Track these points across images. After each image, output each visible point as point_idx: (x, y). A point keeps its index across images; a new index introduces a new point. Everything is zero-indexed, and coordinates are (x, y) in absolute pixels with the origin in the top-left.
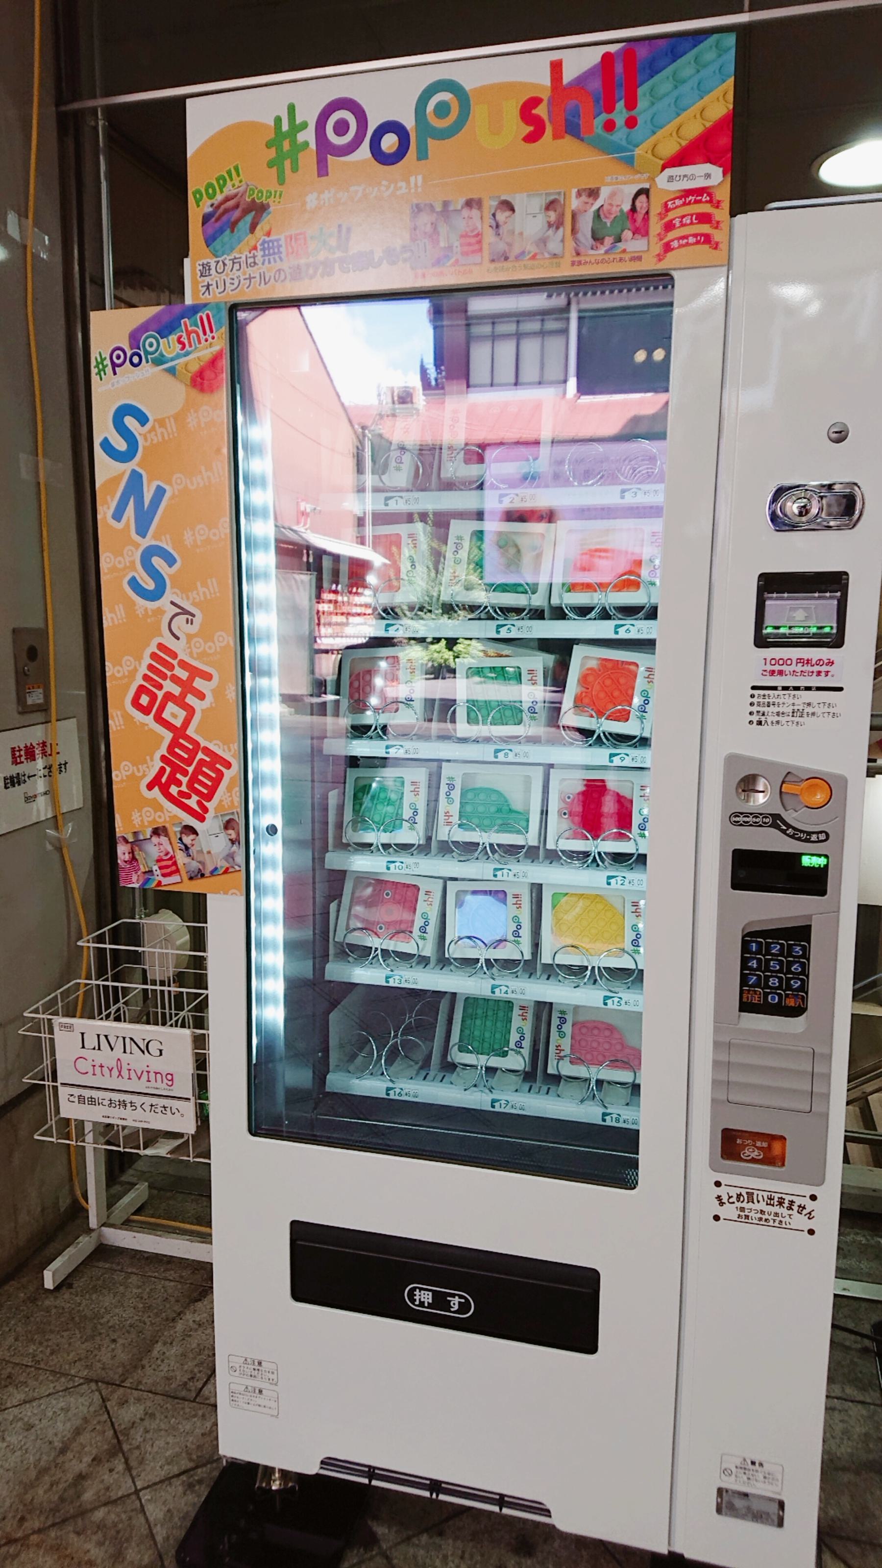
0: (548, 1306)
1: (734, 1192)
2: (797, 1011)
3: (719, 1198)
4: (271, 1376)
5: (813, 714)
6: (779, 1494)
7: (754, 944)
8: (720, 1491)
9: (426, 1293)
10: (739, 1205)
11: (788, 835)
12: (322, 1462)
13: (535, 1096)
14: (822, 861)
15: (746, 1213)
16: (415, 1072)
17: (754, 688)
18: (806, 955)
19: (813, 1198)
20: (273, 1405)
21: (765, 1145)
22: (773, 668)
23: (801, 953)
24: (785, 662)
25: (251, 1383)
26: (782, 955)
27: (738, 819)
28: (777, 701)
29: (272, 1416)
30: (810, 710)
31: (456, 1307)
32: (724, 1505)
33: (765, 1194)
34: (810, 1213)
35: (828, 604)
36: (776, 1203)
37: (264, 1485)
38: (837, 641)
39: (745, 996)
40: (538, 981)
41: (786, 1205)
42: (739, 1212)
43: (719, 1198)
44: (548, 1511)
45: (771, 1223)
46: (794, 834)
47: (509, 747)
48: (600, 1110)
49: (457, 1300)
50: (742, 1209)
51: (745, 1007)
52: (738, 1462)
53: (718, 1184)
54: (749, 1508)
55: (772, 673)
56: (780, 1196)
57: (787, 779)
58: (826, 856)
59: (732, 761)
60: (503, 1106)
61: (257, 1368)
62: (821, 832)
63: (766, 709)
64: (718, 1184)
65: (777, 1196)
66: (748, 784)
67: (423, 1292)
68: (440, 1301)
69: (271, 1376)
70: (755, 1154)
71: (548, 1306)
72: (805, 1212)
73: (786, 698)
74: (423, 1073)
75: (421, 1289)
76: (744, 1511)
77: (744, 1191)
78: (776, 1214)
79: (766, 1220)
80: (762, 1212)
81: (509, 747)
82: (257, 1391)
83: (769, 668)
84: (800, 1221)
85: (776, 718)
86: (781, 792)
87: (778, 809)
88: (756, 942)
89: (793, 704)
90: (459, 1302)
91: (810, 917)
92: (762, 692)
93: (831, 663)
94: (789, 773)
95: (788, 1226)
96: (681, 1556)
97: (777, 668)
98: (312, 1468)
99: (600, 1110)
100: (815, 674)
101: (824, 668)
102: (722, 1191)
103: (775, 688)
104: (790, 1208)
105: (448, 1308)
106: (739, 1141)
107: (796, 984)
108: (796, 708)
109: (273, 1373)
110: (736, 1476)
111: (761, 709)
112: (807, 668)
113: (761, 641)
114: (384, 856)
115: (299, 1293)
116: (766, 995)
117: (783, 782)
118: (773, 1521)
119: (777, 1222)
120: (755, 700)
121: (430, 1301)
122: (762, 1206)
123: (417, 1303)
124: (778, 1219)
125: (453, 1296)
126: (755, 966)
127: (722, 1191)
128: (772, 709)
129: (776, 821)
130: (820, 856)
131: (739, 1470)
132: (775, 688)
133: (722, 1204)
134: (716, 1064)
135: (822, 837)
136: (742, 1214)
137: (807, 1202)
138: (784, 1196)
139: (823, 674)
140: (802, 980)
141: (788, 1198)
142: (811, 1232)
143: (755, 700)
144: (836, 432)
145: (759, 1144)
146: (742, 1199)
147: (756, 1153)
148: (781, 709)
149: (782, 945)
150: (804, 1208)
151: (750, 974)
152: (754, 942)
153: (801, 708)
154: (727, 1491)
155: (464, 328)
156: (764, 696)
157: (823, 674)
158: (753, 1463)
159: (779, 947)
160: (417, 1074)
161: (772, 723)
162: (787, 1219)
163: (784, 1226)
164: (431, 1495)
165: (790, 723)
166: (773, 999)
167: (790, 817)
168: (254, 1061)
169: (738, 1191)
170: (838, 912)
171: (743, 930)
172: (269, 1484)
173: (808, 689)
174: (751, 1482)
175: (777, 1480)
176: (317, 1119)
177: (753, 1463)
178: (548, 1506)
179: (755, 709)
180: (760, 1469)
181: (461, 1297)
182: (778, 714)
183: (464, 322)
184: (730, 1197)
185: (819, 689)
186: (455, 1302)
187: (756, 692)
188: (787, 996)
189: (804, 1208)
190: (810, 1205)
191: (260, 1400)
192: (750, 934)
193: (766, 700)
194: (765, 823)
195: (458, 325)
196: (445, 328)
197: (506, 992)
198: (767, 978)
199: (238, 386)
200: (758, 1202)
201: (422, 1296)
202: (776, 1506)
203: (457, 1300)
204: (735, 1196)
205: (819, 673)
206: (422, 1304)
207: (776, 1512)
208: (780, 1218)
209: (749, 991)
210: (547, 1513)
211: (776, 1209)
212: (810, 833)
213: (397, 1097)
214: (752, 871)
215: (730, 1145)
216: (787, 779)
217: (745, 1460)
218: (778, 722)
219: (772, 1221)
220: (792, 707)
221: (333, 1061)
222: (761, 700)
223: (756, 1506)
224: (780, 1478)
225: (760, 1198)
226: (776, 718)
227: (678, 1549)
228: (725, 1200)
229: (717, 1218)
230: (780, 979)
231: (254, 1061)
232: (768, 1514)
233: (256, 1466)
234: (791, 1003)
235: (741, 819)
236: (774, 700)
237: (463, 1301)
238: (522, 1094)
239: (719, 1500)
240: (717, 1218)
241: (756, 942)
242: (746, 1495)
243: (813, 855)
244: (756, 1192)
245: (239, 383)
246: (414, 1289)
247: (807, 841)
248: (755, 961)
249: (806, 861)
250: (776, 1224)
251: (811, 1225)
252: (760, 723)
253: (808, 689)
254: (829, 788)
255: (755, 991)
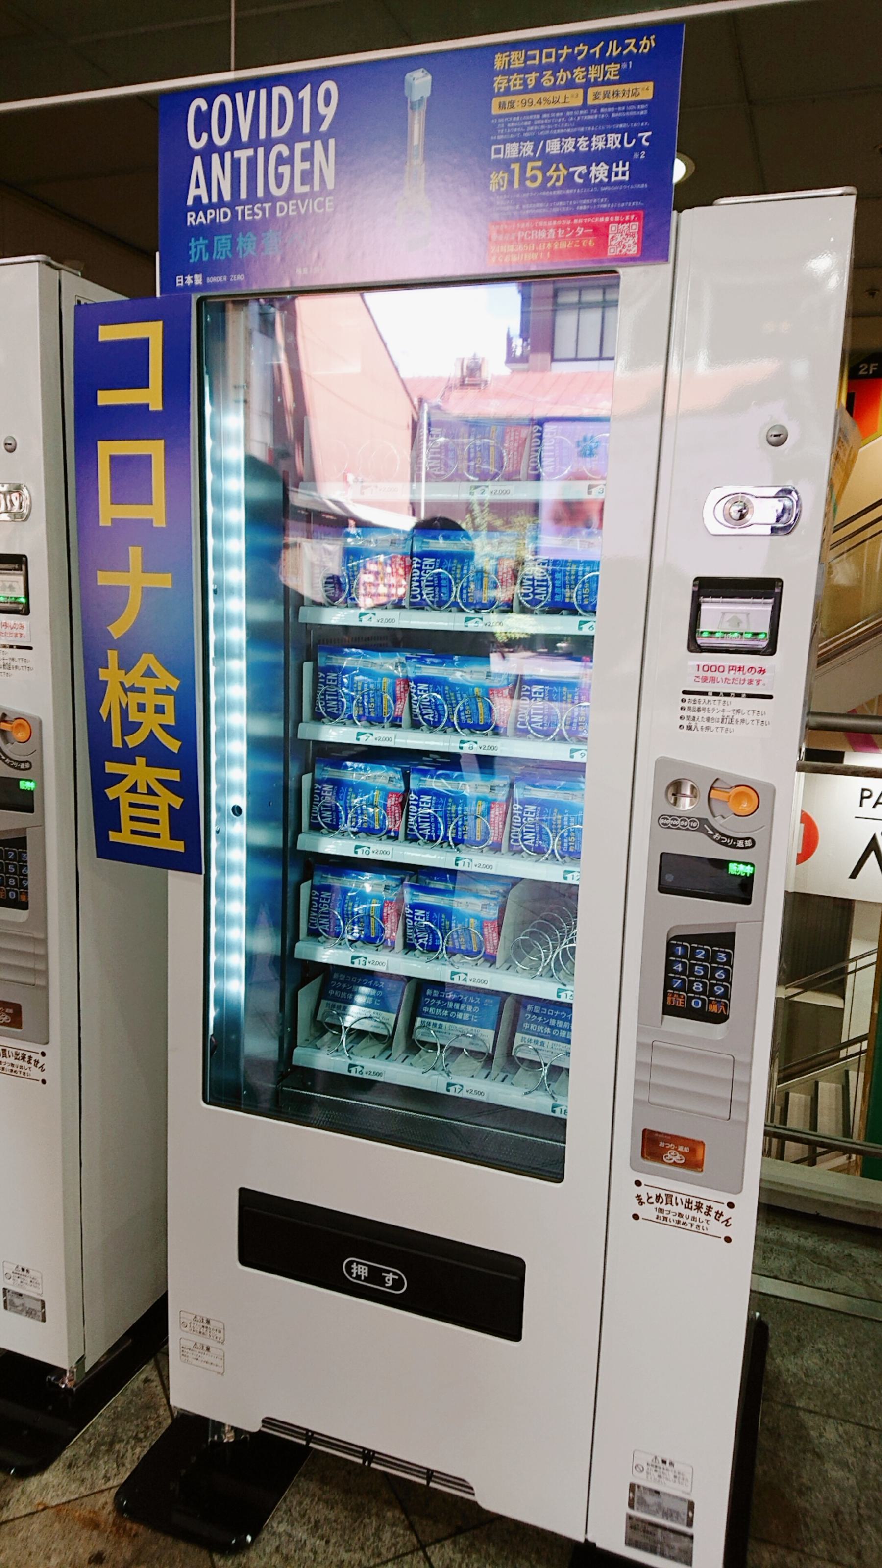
0: (477, 1291)
1: (653, 1193)
2: (720, 1018)
3: (639, 1197)
4: (218, 1335)
5: (743, 721)
6: (689, 1494)
7: (680, 948)
8: (632, 1487)
9: (363, 1267)
10: (658, 1206)
11: (715, 840)
12: (263, 1421)
13: (489, 1083)
14: (749, 870)
15: (665, 1215)
16: (379, 1052)
17: (684, 692)
18: (729, 962)
19: (731, 1205)
20: (221, 1363)
21: (687, 1150)
22: (705, 674)
23: (725, 960)
24: (717, 669)
25: (200, 1340)
26: (706, 960)
27: (667, 822)
28: (707, 706)
29: (219, 1373)
30: (739, 717)
31: (390, 1283)
32: (636, 1499)
33: (684, 1198)
34: (727, 1220)
35: (761, 609)
36: (694, 1207)
37: (216, 1438)
38: (771, 649)
39: (669, 999)
40: (498, 971)
41: (704, 1210)
42: (657, 1213)
43: (639, 1197)
44: (472, 1488)
45: (689, 1227)
46: (721, 839)
47: (475, 739)
48: (549, 1102)
49: (390, 1276)
50: (661, 1211)
51: (668, 1010)
52: (650, 1459)
53: (638, 1183)
54: (659, 1506)
55: (705, 679)
56: (698, 1200)
57: (715, 786)
58: (753, 865)
59: (662, 764)
60: (458, 1090)
61: (205, 1325)
62: (748, 839)
63: (696, 714)
64: (638, 1183)
65: (695, 1200)
66: (676, 787)
67: (359, 1266)
68: (376, 1276)
69: (218, 1335)
70: (677, 1158)
71: (477, 1291)
72: (722, 1219)
73: (717, 703)
74: (387, 1053)
75: (358, 1263)
76: (654, 1508)
77: (663, 1193)
78: (694, 1218)
79: (684, 1223)
80: (680, 1215)
81: (475, 739)
82: (205, 1348)
83: (701, 674)
84: (716, 1227)
85: (706, 724)
86: (709, 799)
87: (706, 814)
88: (682, 946)
89: (723, 711)
90: (393, 1279)
91: (735, 923)
92: (693, 697)
93: (762, 671)
94: (717, 779)
95: (705, 1232)
96: (594, 1544)
97: (709, 674)
98: (255, 1426)
99: (549, 1102)
100: (746, 682)
101: (757, 676)
102: (642, 1191)
103: (706, 694)
104: (707, 1214)
105: (382, 1282)
106: (662, 1144)
107: (719, 991)
108: (726, 714)
109: (220, 1332)
110: (648, 1473)
111: (692, 714)
112: (739, 675)
113: (694, 646)
114: (351, 839)
115: (246, 1258)
116: (690, 999)
117: (712, 788)
118: (683, 1520)
119: (695, 1226)
120: (686, 705)
121: (366, 1275)
122: (680, 1209)
123: (354, 1276)
124: (695, 1223)
125: (388, 1272)
126: (680, 969)
127: (642, 1191)
128: (701, 714)
129: (703, 826)
130: (746, 864)
131: (650, 1467)
132: (706, 694)
133: (641, 1203)
134: (638, 1064)
135: (748, 843)
136: (660, 1215)
137: (724, 1209)
138: (702, 1201)
139: (755, 682)
140: (726, 988)
141: (705, 1204)
142: (728, 1240)
143: (686, 705)
144: (775, 436)
145: (681, 1148)
146: (661, 1200)
147: (678, 1157)
148: (711, 715)
149: (707, 951)
150: (721, 1215)
151: (674, 977)
152: (679, 945)
153: (731, 714)
154: (639, 1487)
155: (550, 313)
156: (695, 700)
157: (755, 682)
158: (664, 1462)
159: (704, 952)
160: (380, 1055)
161: (702, 729)
162: (705, 1224)
163: (701, 1231)
164: (364, 1462)
165: (719, 729)
166: (696, 1004)
167: (717, 823)
168: (211, 1032)
169: (658, 1192)
170: (763, 921)
171: (668, 935)
172: (220, 1437)
173: (738, 695)
174: (662, 1480)
175: (687, 1480)
176: (282, 1090)
177: (664, 1462)
178: (472, 1484)
179: (685, 713)
180: (670, 1468)
181: (395, 1274)
182: (708, 719)
183: (551, 308)
184: (649, 1198)
185: (749, 696)
186: (390, 1278)
187: (687, 697)
188: (710, 1002)
189: (721, 1215)
190: (727, 1212)
191: (206, 1358)
192: (676, 938)
193: (697, 705)
194: (693, 827)
195: (546, 311)
196: (531, 314)
197: (465, 980)
198: (691, 983)
199: (206, 378)
200: (677, 1204)
201: (359, 1270)
202: (686, 1505)
203: (390, 1276)
204: (654, 1197)
205: (751, 682)
206: (358, 1277)
207: (686, 1511)
208: (698, 1223)
209: (673, 994)
210: (469, 1489)
211: (694, 1213)
212: (736, 839)
213: (358, 1075)
214: (678, 876)
215: (652, 1145)
216: (715, 786)
217: (656, 1458)
218: (707, 728)
219: (689, 1225)
220: (721, 714)
221: (300, 1038)
222: (692, 705)
223: (667, 1504)
224: (689, 1477)
225: (679, 1201)
226: (706, 724)
227: (591, 1538)
228: (644, 1200)
229: (636, 1217)
230: (704, 984)
231: (211, 1032)
232: (678, 1513)
233: (206, 1420)
234: (714, 1008)
235: (669, 821)
236: (704, 705)
237: (397, 1277)
238: (477, 1080)
239: (631, 1495)
240: (636, 1217)
241: (682, 946)
242: (657, 1492)
243: (739, 863)
244: (675, 1195)
245: (207, 373)
246: (352, 1262)
247: (734, 847)
248: (680, 965)
249: (733, 869)
250: (694, 1228)
251: (727, 1232)
252: (689, 728)
253: (738, 695)
254: (754, 796)
255: (679, 995)
